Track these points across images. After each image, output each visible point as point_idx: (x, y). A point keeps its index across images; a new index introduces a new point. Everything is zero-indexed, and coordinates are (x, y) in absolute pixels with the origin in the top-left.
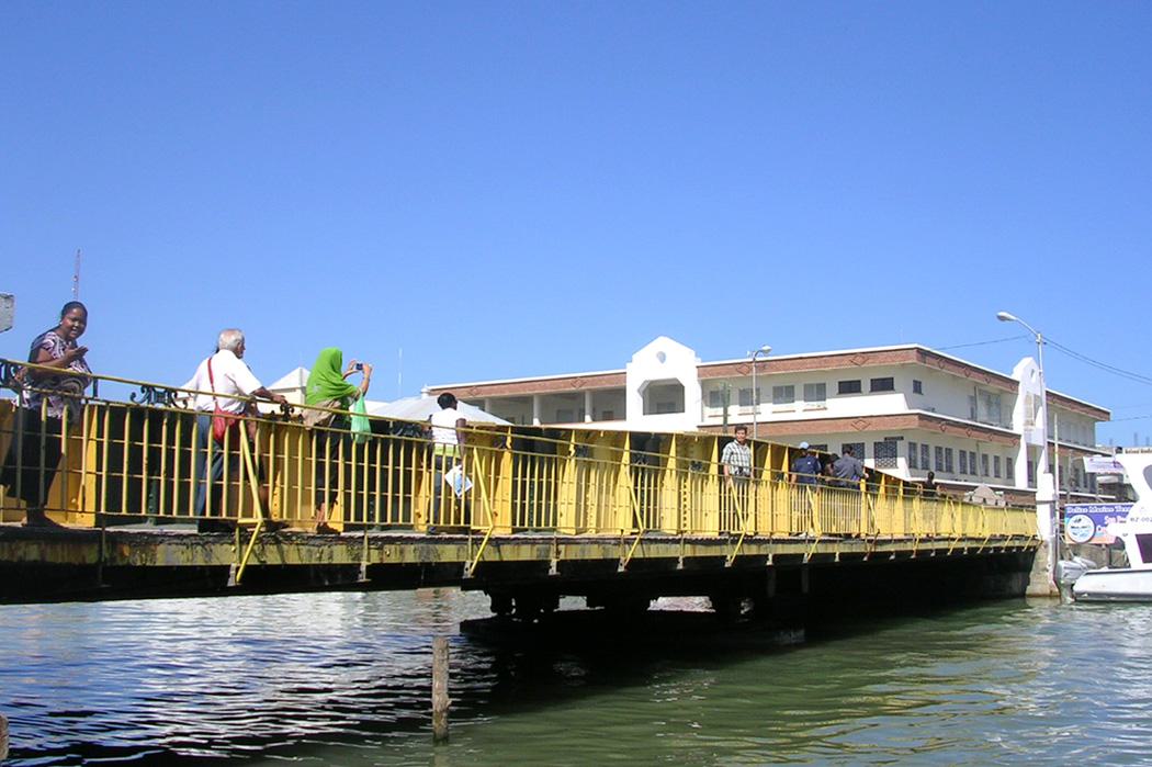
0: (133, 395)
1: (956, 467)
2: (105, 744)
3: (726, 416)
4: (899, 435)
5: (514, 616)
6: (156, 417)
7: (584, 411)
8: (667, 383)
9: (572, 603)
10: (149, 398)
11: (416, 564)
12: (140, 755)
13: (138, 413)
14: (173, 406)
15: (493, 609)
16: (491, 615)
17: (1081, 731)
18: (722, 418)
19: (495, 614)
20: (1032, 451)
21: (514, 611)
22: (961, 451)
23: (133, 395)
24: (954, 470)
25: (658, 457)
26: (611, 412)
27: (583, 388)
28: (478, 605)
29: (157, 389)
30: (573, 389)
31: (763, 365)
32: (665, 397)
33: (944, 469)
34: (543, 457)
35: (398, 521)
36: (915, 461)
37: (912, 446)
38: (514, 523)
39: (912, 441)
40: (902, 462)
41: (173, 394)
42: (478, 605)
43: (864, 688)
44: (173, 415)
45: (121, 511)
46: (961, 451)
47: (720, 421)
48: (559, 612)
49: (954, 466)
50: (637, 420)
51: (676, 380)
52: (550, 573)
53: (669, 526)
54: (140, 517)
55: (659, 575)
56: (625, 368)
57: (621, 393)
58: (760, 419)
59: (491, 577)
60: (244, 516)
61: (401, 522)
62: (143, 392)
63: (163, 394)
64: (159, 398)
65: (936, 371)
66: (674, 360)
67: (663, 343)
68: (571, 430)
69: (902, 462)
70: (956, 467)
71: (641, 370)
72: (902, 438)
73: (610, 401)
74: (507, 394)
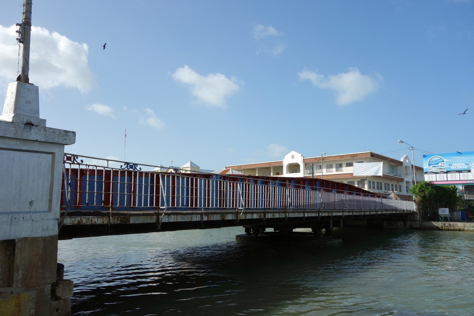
0: (121, 166)
1: (383, 188)
4: (366, 179)
5: (252, 234)
6: (130, 173)
7: (271, 172)
8: (294, 164)
10: (127, 166)
11: (272, 218)
12: (146, 285)
13: (123, 172)
14: (136, 170)
15: (245, 232)
19: (246, 233)
22: (392, 184)
23: (121, 166)
26: (279, 173)
27: (271, 166)
29: (130, 164)
30: (268, 166)
31: (324, 159)
32: (294, 168)
37: (370, 182)
39: (369, 180)
41: (136, 166)
44: (82, 170)
46: (392, 184)
50: (286, 174)
53: (201, 203)
54: (257, 208)
56: (283, 160)
57: (281, 167)
60: (161, 206)
62: (125, 165)
63: (133, 166)
64: (131, 167)
66: (298, 159)
67: (293, 153)
70: (383, 188)
71: (287, 161)
72: (366, 180)
73: (279, 168)
74: (249, 168)
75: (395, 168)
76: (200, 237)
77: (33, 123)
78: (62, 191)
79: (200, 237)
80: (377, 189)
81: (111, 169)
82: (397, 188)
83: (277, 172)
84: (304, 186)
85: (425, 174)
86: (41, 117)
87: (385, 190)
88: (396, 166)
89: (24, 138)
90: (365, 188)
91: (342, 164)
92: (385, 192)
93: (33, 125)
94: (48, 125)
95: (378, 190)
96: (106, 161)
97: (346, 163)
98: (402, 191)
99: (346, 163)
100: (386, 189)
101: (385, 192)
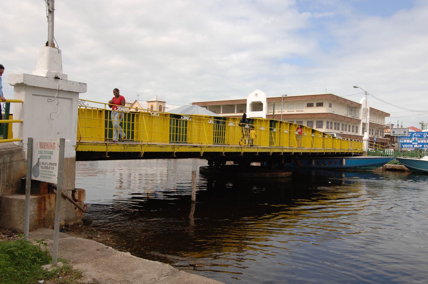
2: (369, 168)
3: (274, 112)
8: (257, 103)
9: (228, 163)
16: (208, 165)
17: (42, 276)
18: (273, 113)
20: (364, 124)
21: (214, 164)
24: (351, 131)
25: (225, 122)
27: (235, 103)
28: (205, 163)
30: (232, 104)
33: (337, 129)
34: (178, 120)
35: (218, 143)
36: (336, 128)
38: (170, 140)
40: (324, 126)
42: (205, 163)
43: (351, 177)
45: (177, 141)
47: (272, 114)
48: (226, 165)
49: (351, 130)
51: (261, 102)
52: (282, 154)
55: (252, 156)
57: (245, 105)
58: (283, 113)
59: (207, 155)
61: (181, 141)
65: (381, 115)
67: (257, 91)
68: (257, 119)
69: (324, 126)
71: (250, 100)
75: (353, 109)
76: (175, 172)
77: (59, 77)
78: (181, 115)
79: (175, 172)
80: (334, 129)
81: (97, 109)
82: (354, 129)
83: (327, 121)
84: (271, 128)
85: (153, 110)
86: (63, 73)
87: (342, 130)
88: (355, 108)
89: (78, 91)
90: (313, 128)
91: (323, 103)
92: (341, 132)
93: (59, 79)
94: (69, 79)
95: (353, 133)
96: (104, 104)
97: (307, 104)
98: (262, 117)
99: (307, 104)
100: (343, 130)
101: (341, 132)
